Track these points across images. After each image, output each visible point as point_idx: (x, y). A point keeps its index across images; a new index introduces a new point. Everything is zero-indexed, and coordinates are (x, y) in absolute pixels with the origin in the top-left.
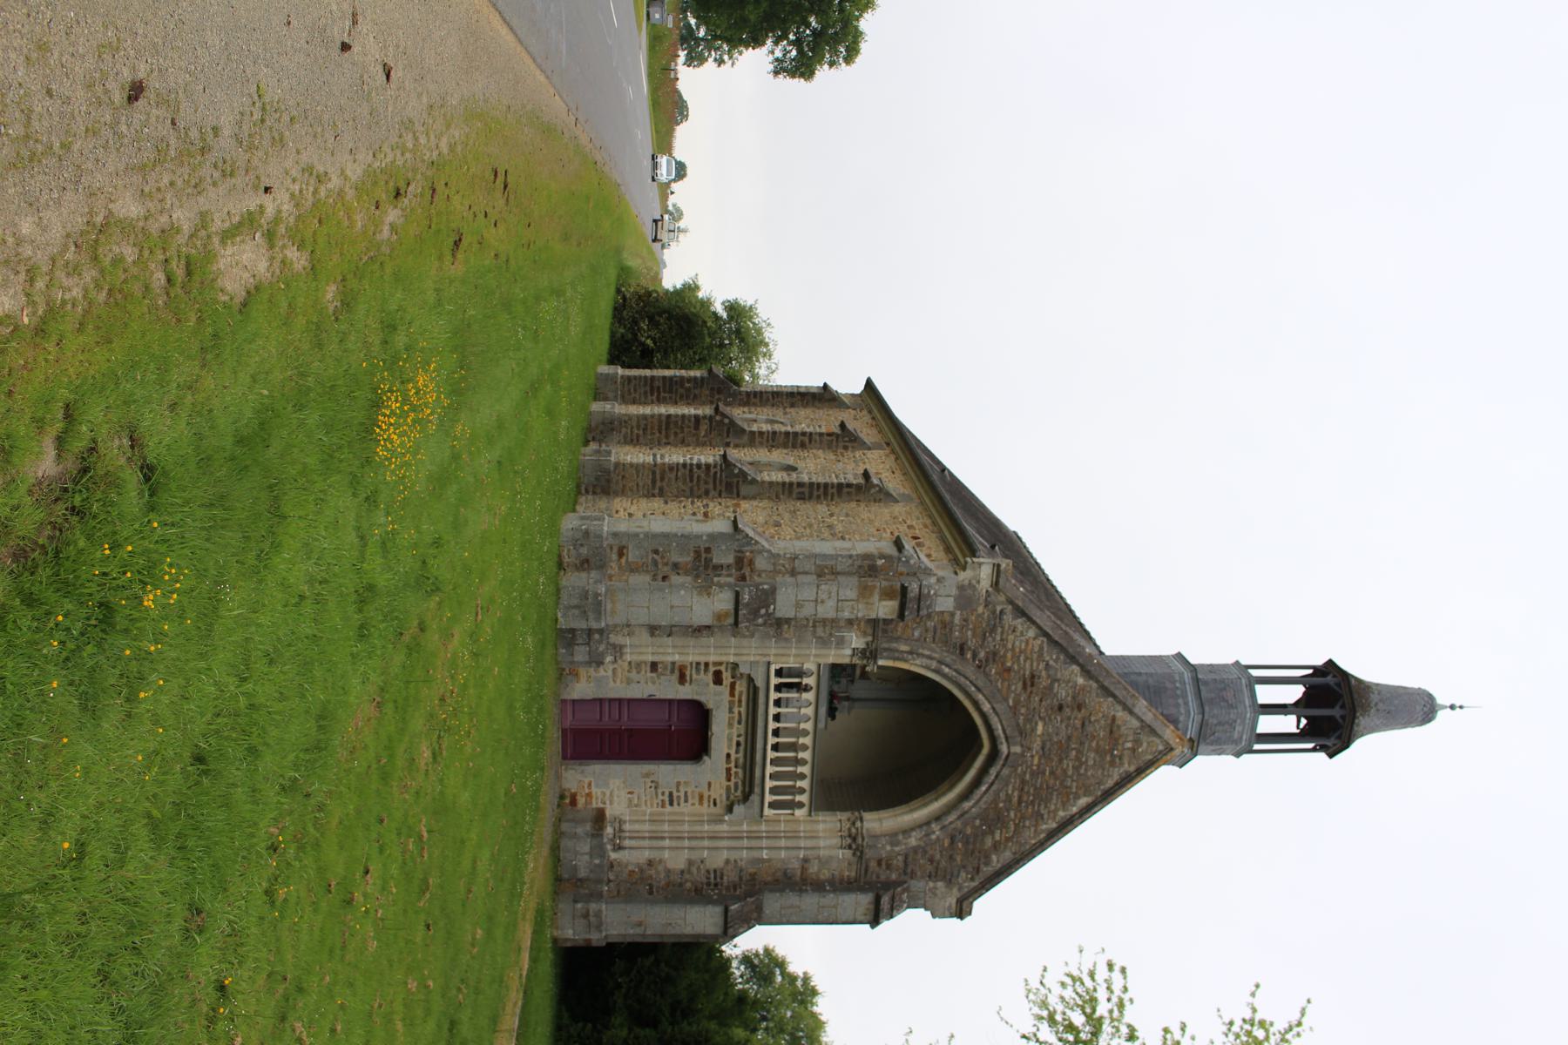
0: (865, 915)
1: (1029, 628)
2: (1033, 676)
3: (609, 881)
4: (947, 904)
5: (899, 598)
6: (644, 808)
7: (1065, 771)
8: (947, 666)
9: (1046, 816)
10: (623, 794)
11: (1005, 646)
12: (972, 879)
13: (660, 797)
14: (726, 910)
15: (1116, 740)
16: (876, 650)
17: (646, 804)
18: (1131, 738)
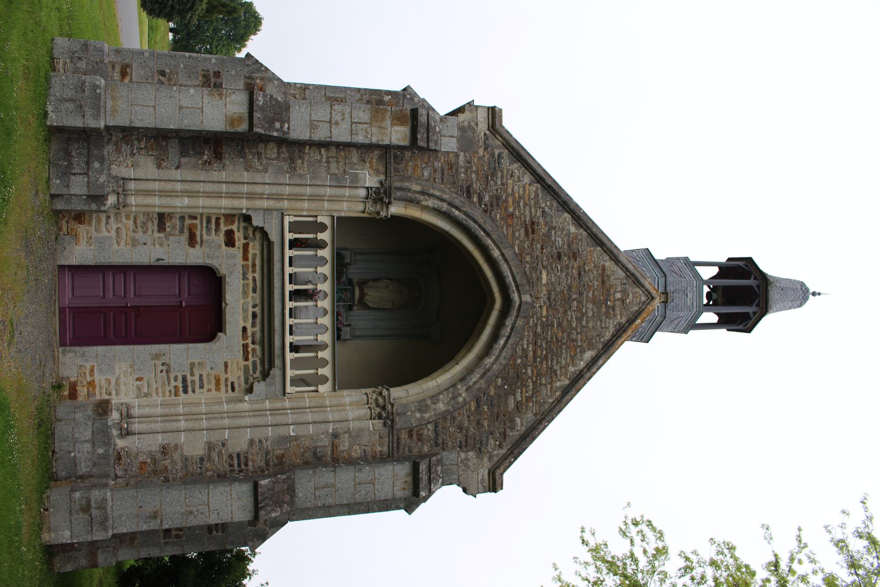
0: (404, 489)
1: (524, 174)
2: (533, 223)
3: (116, 477)
4: (480, 477)
5: (410, 123)
6: (155, 397)
7: (569, 322)
8: (457, 208)
9: (558, 372)
10: (131, 380)
11: (506, 191)
12: (500, 446)
13: (173, 383)
14: (256, 486)
15: (608, 291)
16: (390, 187)
17: (157, 394)
18: (619, 289)
